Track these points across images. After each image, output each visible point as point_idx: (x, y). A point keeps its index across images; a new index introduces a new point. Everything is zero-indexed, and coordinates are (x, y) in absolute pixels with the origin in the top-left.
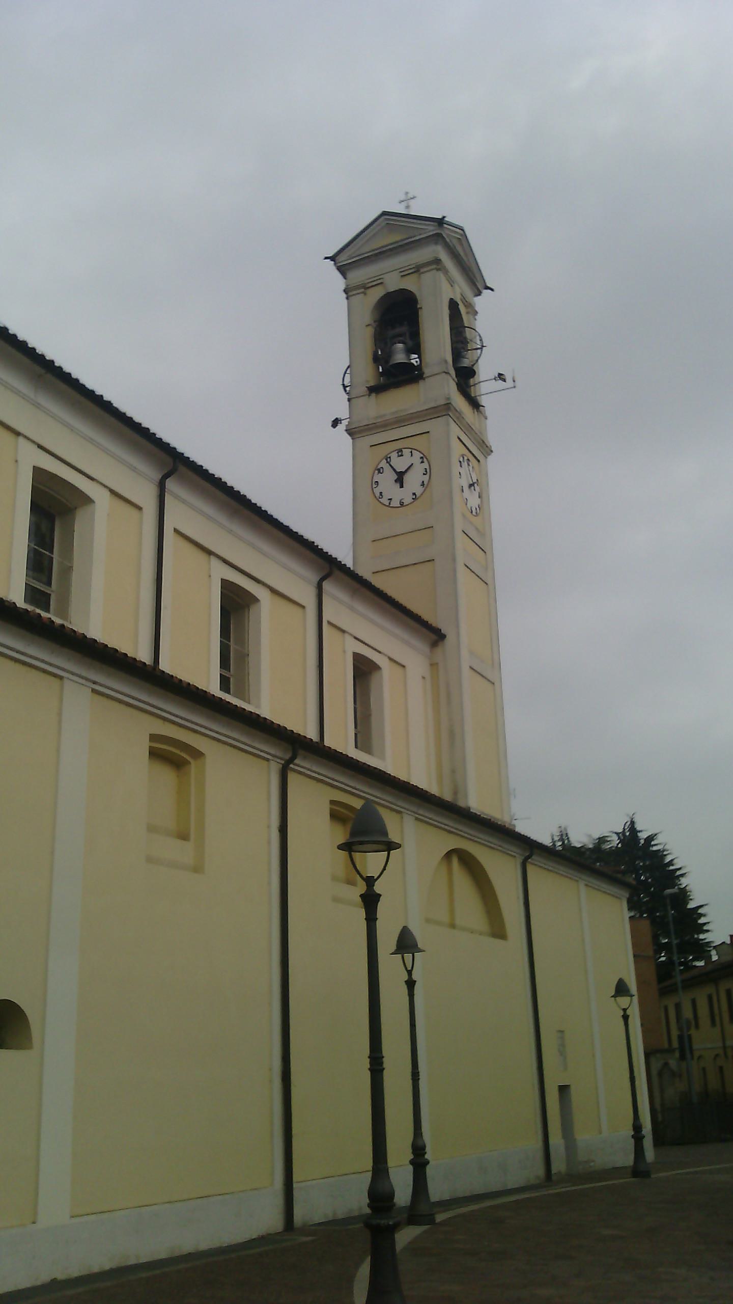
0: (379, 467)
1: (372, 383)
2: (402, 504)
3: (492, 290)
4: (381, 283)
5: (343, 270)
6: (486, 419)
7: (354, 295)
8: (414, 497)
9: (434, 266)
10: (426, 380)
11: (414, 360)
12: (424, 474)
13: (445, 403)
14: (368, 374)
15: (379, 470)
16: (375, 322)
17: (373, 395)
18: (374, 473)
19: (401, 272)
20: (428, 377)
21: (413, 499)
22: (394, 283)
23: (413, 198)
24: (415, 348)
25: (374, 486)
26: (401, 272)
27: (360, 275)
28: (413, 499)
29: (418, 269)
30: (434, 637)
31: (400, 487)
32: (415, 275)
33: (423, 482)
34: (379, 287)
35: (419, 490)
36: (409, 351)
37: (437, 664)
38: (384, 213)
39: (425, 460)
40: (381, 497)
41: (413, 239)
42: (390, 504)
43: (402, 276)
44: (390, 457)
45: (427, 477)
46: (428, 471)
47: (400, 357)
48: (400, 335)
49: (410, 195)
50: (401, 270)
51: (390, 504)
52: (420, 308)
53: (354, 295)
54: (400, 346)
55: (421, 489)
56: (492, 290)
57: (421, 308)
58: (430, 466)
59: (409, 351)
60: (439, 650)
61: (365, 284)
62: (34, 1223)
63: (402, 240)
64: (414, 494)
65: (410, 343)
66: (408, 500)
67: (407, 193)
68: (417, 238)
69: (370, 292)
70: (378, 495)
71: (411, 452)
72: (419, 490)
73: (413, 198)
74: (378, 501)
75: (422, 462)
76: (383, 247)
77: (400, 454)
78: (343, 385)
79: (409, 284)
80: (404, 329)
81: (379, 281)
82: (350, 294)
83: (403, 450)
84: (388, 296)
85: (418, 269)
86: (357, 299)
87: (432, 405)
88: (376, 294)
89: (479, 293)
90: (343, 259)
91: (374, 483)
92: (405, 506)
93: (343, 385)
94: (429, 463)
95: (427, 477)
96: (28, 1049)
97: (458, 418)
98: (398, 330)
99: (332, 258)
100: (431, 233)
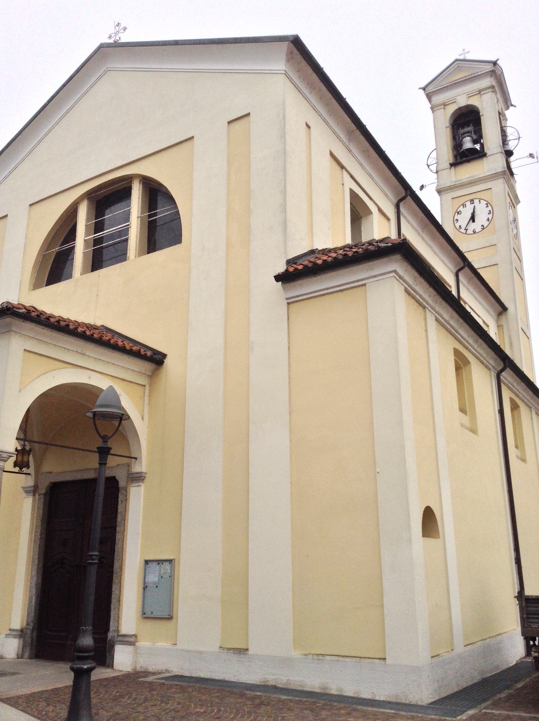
0: (458, 210)
1: (451, 161)
2: (474, 232)
3: (515, 107)
4: (455, 102)
5: (429, 96)
6: (516, 183)
7: (484, 94)
8: (483, 227)
9: (491, 90)
10: (488, 157)
11: (478, 147)
12: (489, 214)
13: (502, 170)
14: (448, 155)
15: (458, 213)
16: (451, 125)
17: (453, 168)
18: (455, 214)
19: (467, 95)
20: (489, 156)
21: (482, 228)
22: (463, 102)
23: (469, 52)
24: (478, 138)
25: (455, 222)
26: (467, 95)
27: (438, 99)
28: (482, 228)
29: (480, 92)
30: (500, 309)
31: (473, 222)
32: (479, 95)
33: (488, 218)
34: (455, 104)
35: (486, 224)
36: (475, 142)
37: (502, 326)
38: (456, 60)
39: (489, 205)
40: (460, 228)
41: (476, 74)
42: (466, 232)
43: (469, 97)
44: (465, 205)
45: (491, 215)
46: (491, 211)
47: (468, 144)
48: (468, 132)
49: (466, 51)
50: (468, 94)
51: (466, 232)
52: (482, 115)
53: (484, 94)
54: (468, 139)
55: (487, 223)
56: (515, 107)
57: (483, 115)
58: (492, 208)
59: (475, 142)
60: (503, 318)
61: (444, 103)
62: (452, 650)
63: (469, 75)
64: (482, 226)
65: (475, 137)
66: (478, 229)
67: (464, 50)
68: (479, 73)
69: (448, 107)
70: (458, 227)
71: (480, 201)
72: (486, 224)
73: (469, 52)
74: (458, 231)
75: (487, 207)
76: (456, 80)
77: (472, 202)
78: (427, 164)
79: (474, 102)
80: (470, 128)
81: (454, 101)
82: (435, 109)
83: (474, 200)
84: (460, 109)
85: (480, 92)
86: (440, 112)
87: (494, 172)
88: (452, 109)
89: (507, 108)
90: (430, 89)
91: (455, 220)
92: (477, 233)
93: (427, 164)
94: (491, 206)
95: (491, 215)
96: (435, 537)
97: (508, 180)
98: (467, 129)
99: (424, 89)
100: (487, 71)
